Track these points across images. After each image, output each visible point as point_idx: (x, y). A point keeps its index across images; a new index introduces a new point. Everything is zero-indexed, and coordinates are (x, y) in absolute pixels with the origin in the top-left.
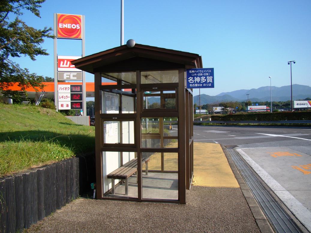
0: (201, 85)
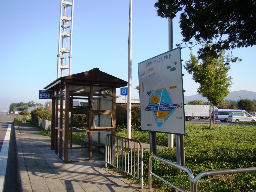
0: (46, 98)
